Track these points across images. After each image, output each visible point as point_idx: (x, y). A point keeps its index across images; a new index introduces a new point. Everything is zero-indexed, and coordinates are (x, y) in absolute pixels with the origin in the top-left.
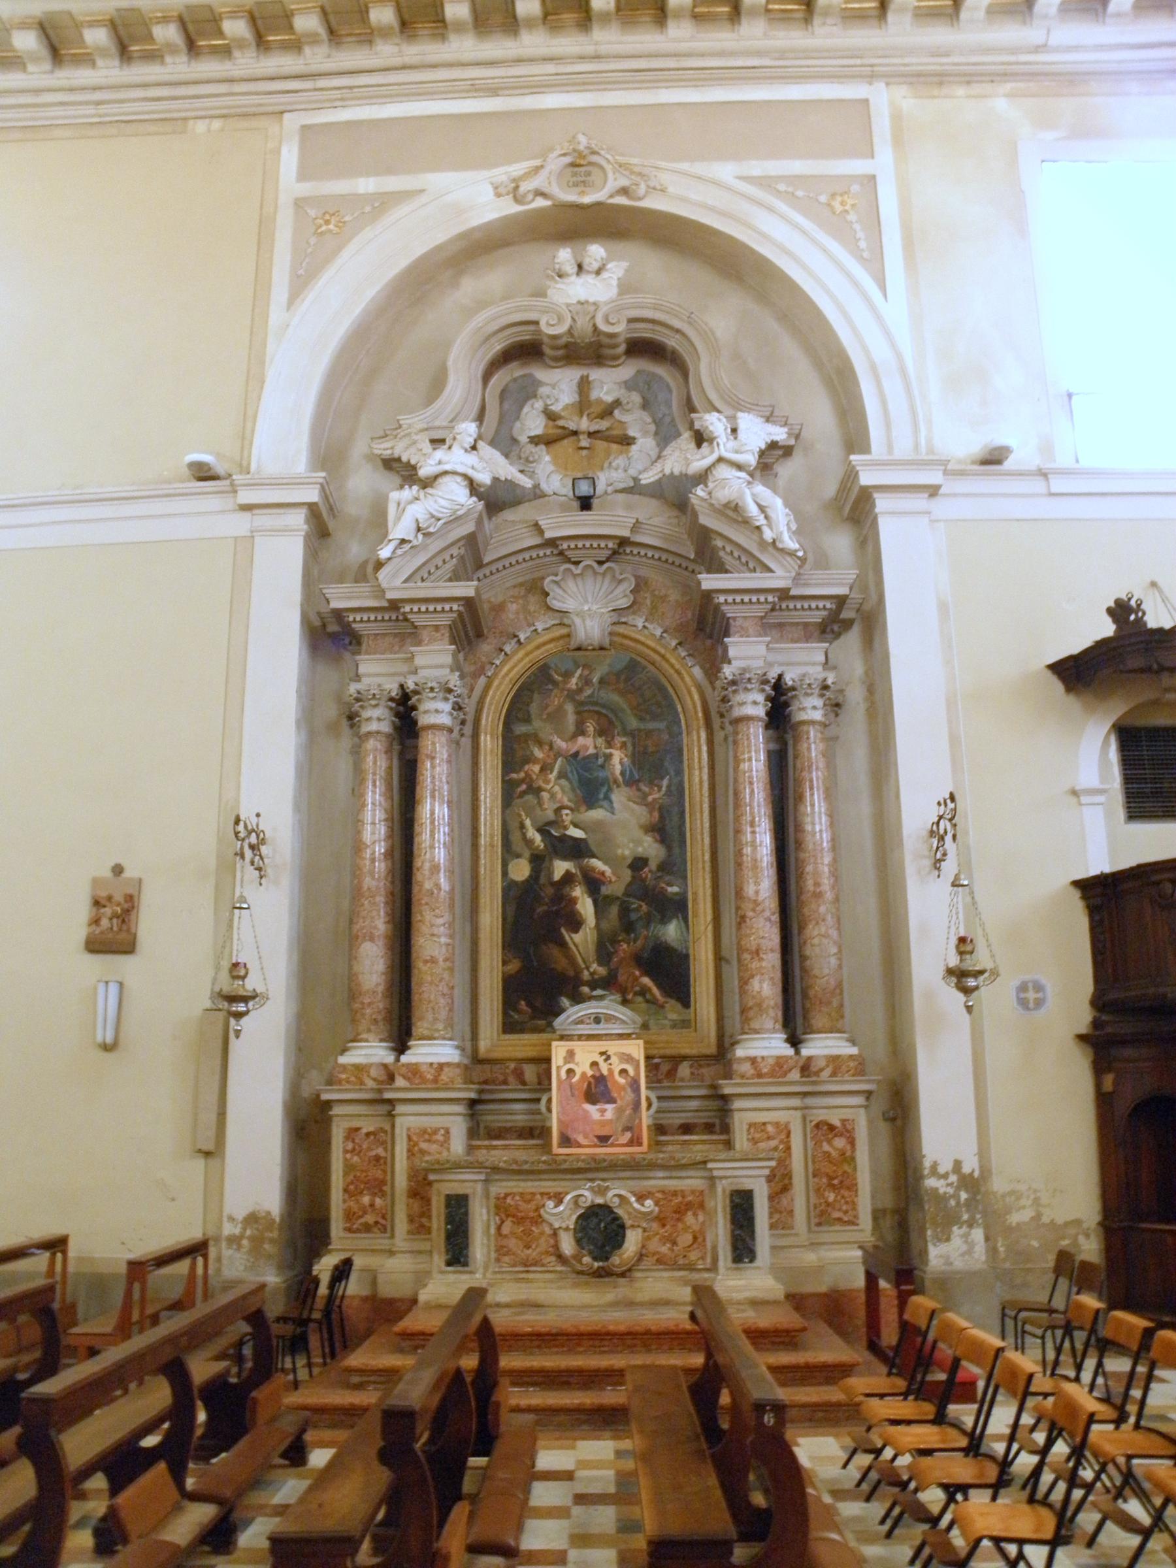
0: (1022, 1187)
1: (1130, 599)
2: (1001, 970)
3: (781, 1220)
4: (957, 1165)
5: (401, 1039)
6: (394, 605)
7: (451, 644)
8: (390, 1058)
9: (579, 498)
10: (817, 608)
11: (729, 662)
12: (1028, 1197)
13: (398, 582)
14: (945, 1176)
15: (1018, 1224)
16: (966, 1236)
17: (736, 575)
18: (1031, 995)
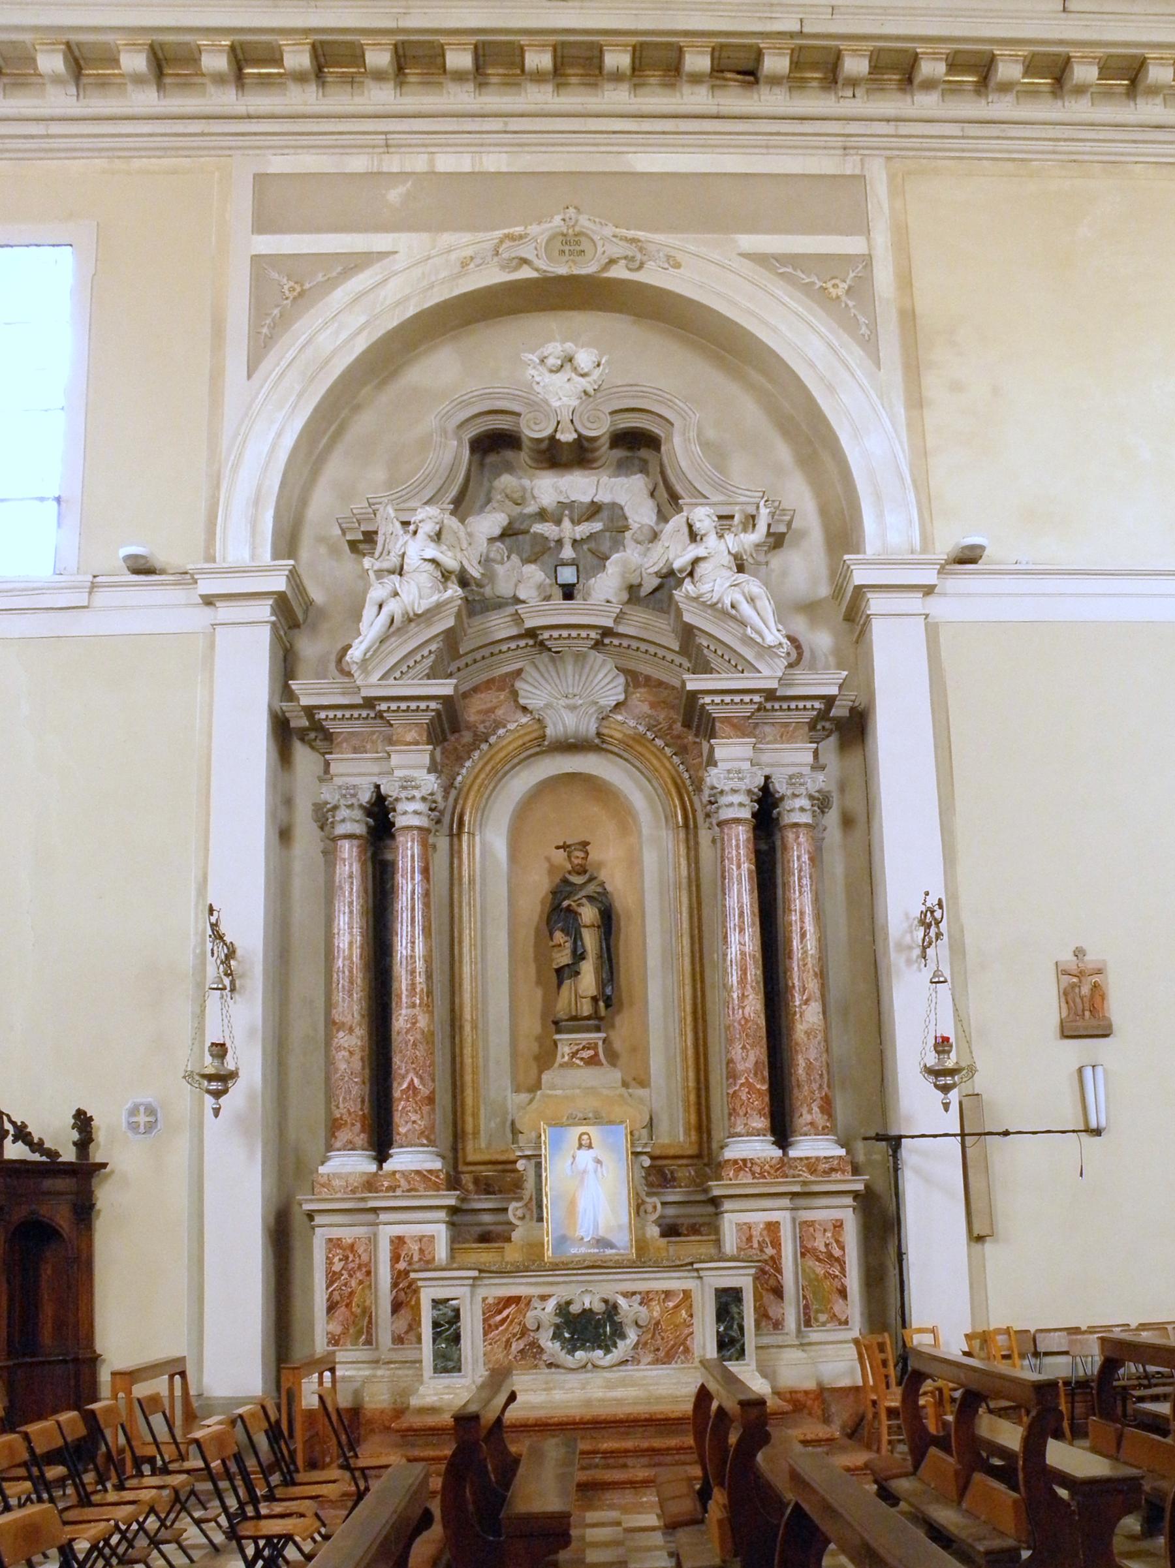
3: (768, 1321)
5: (381, 1146)
6: (370, 703)
7: (428, 744)
8: (373, 1167)
9: (563, 586)
10: (805, 708)
11: (715, 765)
13: (374, 678)
17: (724, 675)
18: (142, 1119)
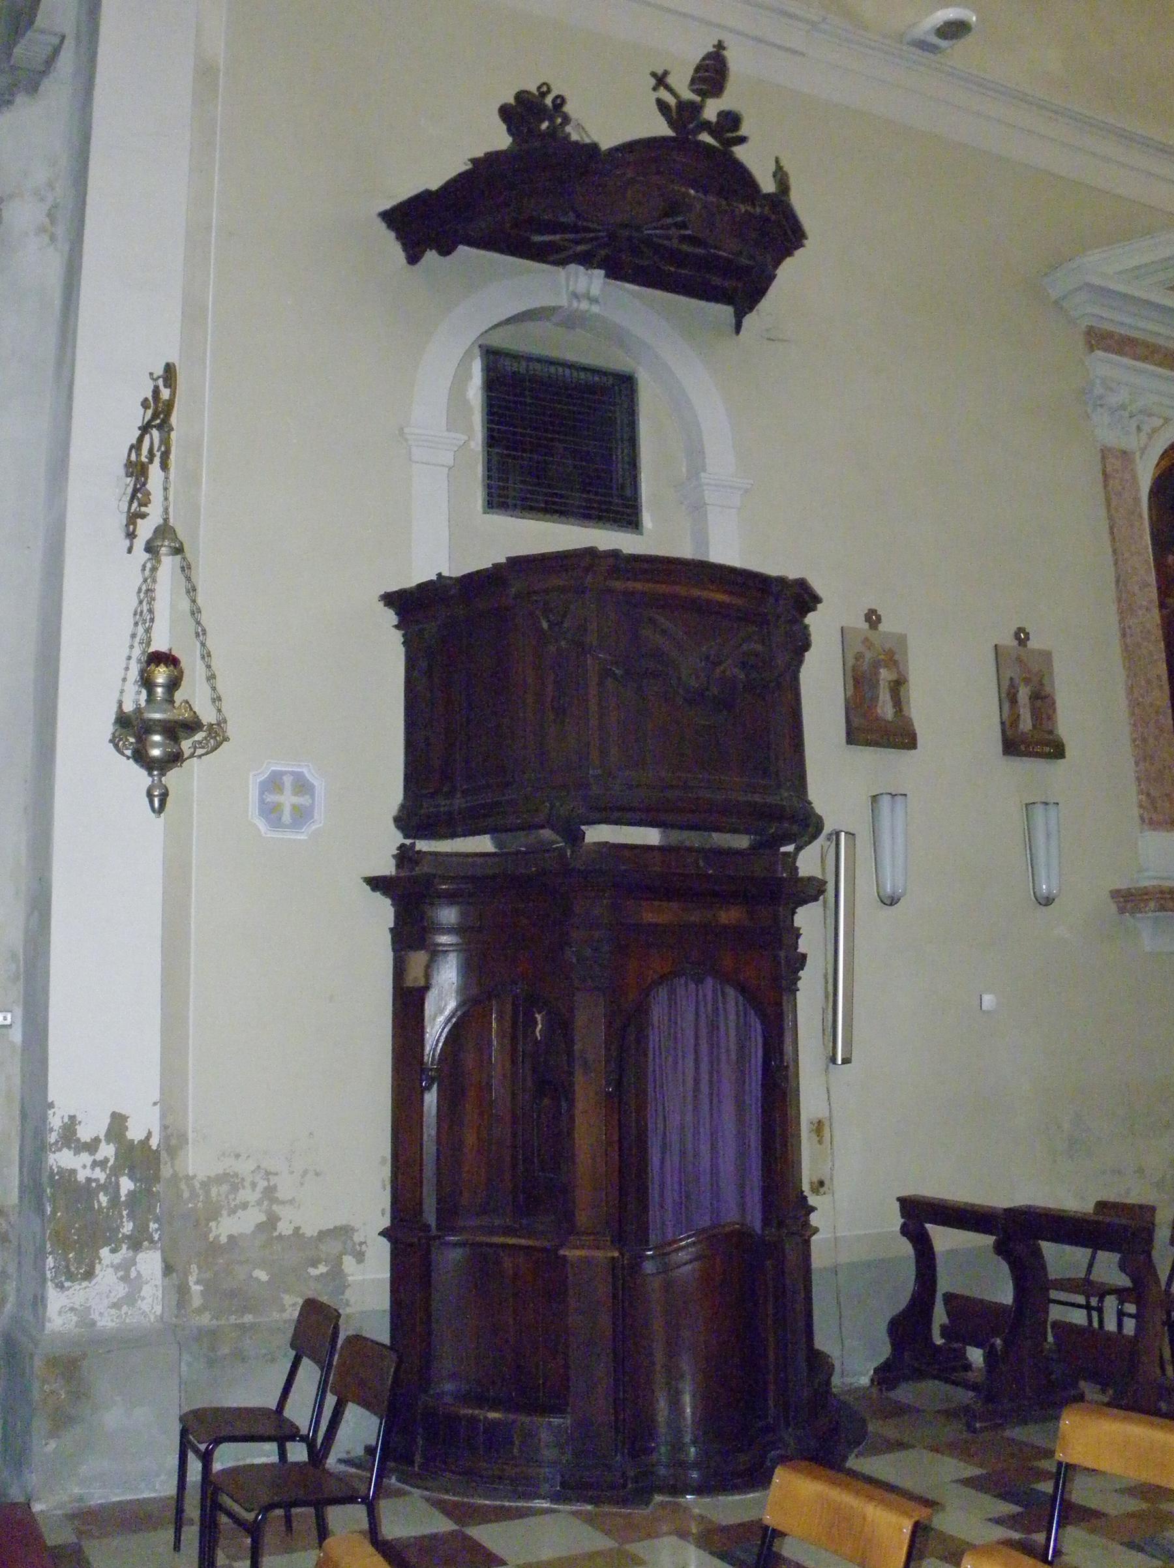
0: (244, 1168)
1: (543, 95)
2: (231, 729)
4: (118, 1123)
12: (254, 1185)
14: (92, 1146)
15: (231, 1237)
16: (124, 1269)
